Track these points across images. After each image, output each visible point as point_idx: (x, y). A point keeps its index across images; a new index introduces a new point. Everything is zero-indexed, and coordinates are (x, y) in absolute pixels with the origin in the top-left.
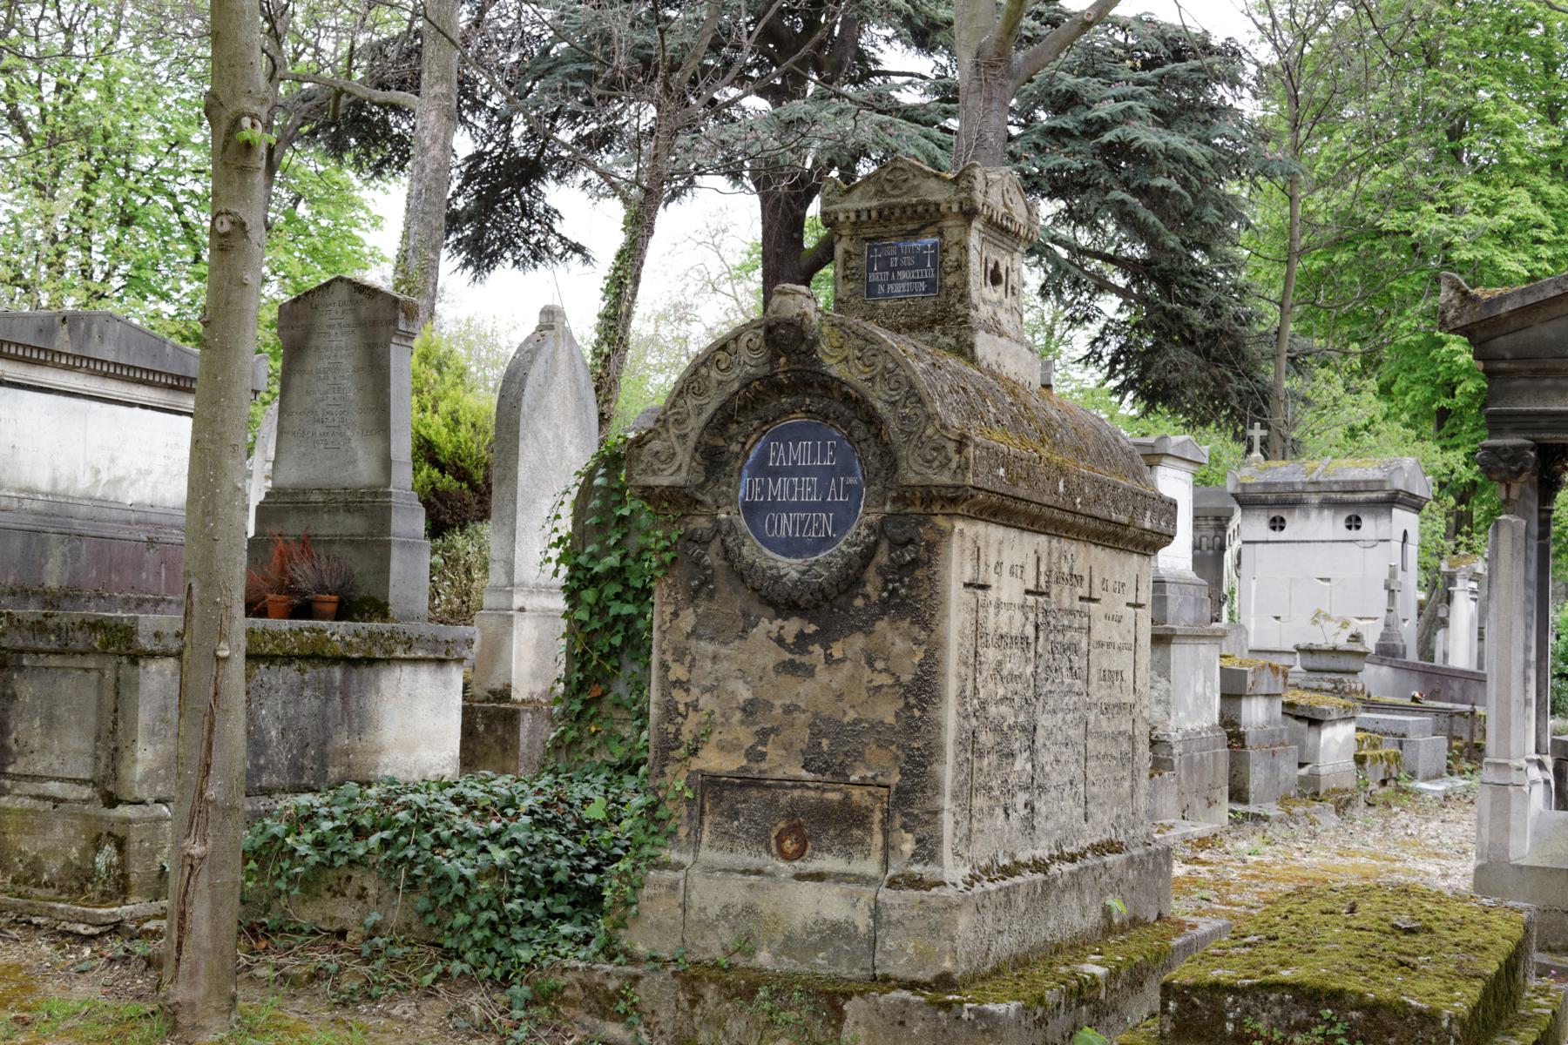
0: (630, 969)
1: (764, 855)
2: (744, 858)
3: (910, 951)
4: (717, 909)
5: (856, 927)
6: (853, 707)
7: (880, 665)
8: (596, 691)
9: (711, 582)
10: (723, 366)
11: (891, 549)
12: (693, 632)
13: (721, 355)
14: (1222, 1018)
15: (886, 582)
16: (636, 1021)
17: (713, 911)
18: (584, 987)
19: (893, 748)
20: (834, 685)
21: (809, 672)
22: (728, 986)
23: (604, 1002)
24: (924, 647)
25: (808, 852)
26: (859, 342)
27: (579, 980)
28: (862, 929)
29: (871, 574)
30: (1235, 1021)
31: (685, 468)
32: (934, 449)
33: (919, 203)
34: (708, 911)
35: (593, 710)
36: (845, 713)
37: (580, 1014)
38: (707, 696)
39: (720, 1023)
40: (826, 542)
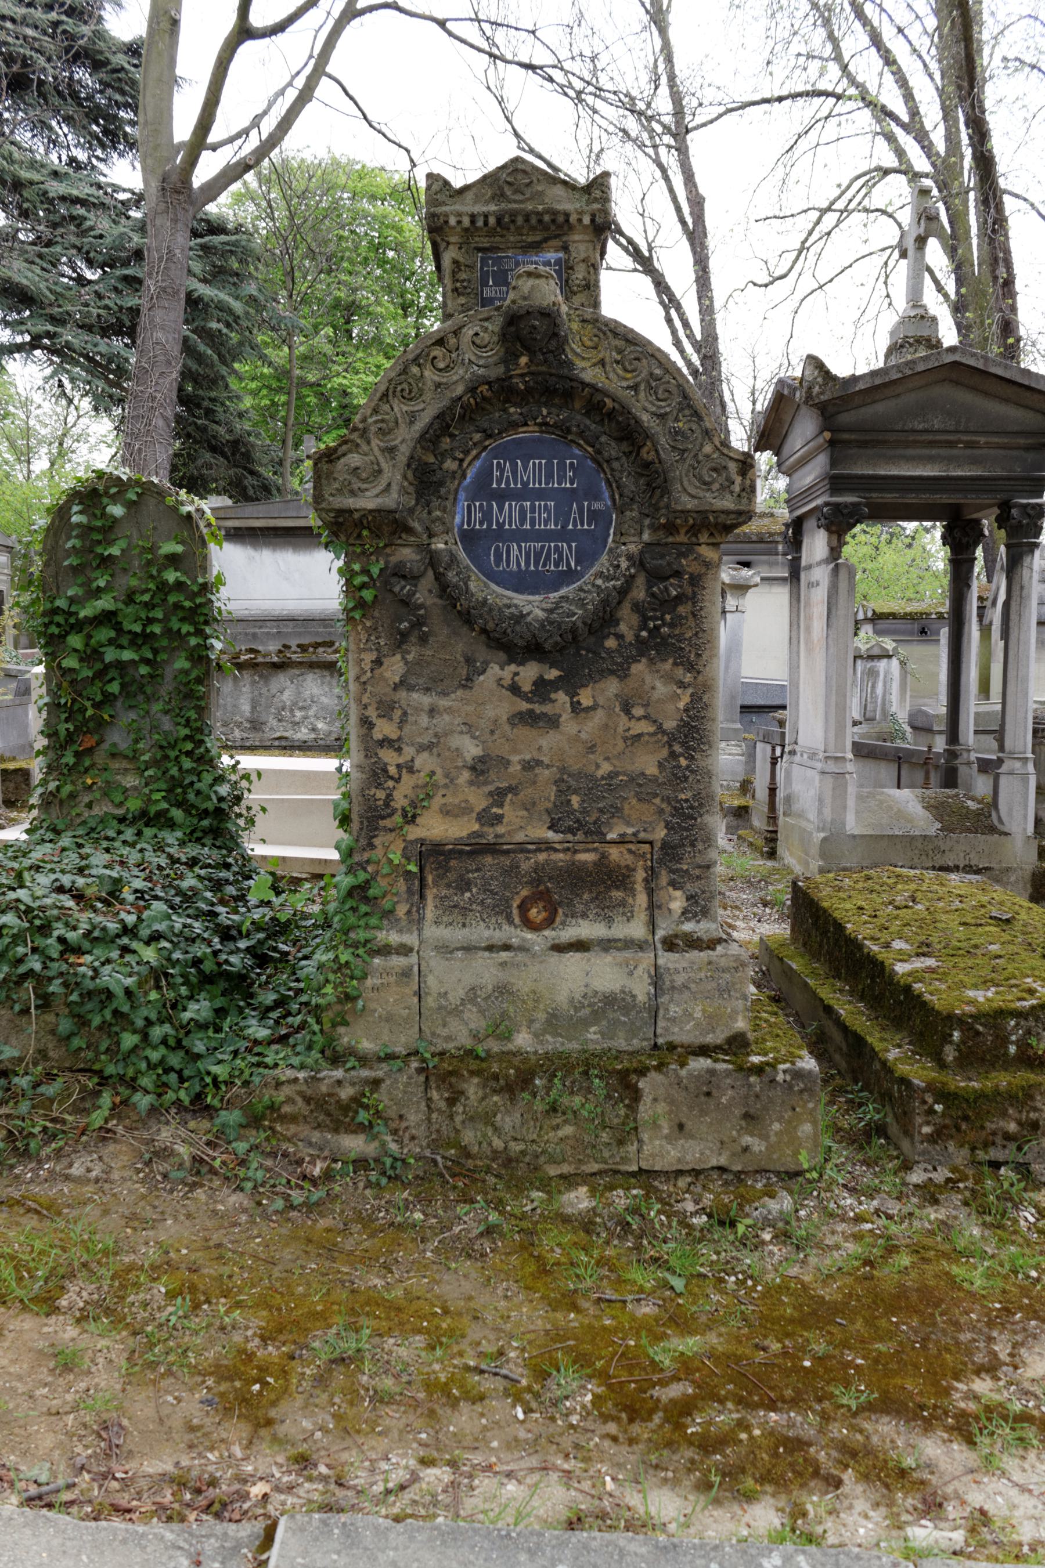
0: (365, 1073)
1: (506, 927)
2: (481, 932)
3: (698, 1015)
4: (461, 993)
5: (634, 997)
6: (607, 759)
7: (638, 711)
8: (89, 741)
9: (424, 624)
10: (441, 365)
11: (649, 585)
12: (402, 682)
13: (437, 352)
14: (1005, 1041)
15: (645, 619)
16: (382, 1129)
17: (457, 994)
18: (308, 1100)
19: (657, 801)
20: (584, 736)
21: (553, 722)
22: (496, 1077)
23: (337, 1113)
24: (690, 691)
25: (558, 920)
26: (620, 343)
27: (300, 1093)
28: (641, 998)
29: (625, 612)
30: (1016, 1043)
31: (395, 488)
32: (714, 470)
33: (547, 211)
34: (450, 997)
35: (87, 763)
36: (598, 766)
37: (304, 1130)
38: (425, 755)
39: (488, 1118)
40: (569, 576)
